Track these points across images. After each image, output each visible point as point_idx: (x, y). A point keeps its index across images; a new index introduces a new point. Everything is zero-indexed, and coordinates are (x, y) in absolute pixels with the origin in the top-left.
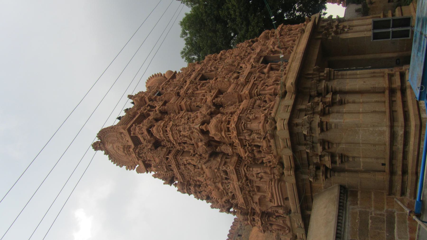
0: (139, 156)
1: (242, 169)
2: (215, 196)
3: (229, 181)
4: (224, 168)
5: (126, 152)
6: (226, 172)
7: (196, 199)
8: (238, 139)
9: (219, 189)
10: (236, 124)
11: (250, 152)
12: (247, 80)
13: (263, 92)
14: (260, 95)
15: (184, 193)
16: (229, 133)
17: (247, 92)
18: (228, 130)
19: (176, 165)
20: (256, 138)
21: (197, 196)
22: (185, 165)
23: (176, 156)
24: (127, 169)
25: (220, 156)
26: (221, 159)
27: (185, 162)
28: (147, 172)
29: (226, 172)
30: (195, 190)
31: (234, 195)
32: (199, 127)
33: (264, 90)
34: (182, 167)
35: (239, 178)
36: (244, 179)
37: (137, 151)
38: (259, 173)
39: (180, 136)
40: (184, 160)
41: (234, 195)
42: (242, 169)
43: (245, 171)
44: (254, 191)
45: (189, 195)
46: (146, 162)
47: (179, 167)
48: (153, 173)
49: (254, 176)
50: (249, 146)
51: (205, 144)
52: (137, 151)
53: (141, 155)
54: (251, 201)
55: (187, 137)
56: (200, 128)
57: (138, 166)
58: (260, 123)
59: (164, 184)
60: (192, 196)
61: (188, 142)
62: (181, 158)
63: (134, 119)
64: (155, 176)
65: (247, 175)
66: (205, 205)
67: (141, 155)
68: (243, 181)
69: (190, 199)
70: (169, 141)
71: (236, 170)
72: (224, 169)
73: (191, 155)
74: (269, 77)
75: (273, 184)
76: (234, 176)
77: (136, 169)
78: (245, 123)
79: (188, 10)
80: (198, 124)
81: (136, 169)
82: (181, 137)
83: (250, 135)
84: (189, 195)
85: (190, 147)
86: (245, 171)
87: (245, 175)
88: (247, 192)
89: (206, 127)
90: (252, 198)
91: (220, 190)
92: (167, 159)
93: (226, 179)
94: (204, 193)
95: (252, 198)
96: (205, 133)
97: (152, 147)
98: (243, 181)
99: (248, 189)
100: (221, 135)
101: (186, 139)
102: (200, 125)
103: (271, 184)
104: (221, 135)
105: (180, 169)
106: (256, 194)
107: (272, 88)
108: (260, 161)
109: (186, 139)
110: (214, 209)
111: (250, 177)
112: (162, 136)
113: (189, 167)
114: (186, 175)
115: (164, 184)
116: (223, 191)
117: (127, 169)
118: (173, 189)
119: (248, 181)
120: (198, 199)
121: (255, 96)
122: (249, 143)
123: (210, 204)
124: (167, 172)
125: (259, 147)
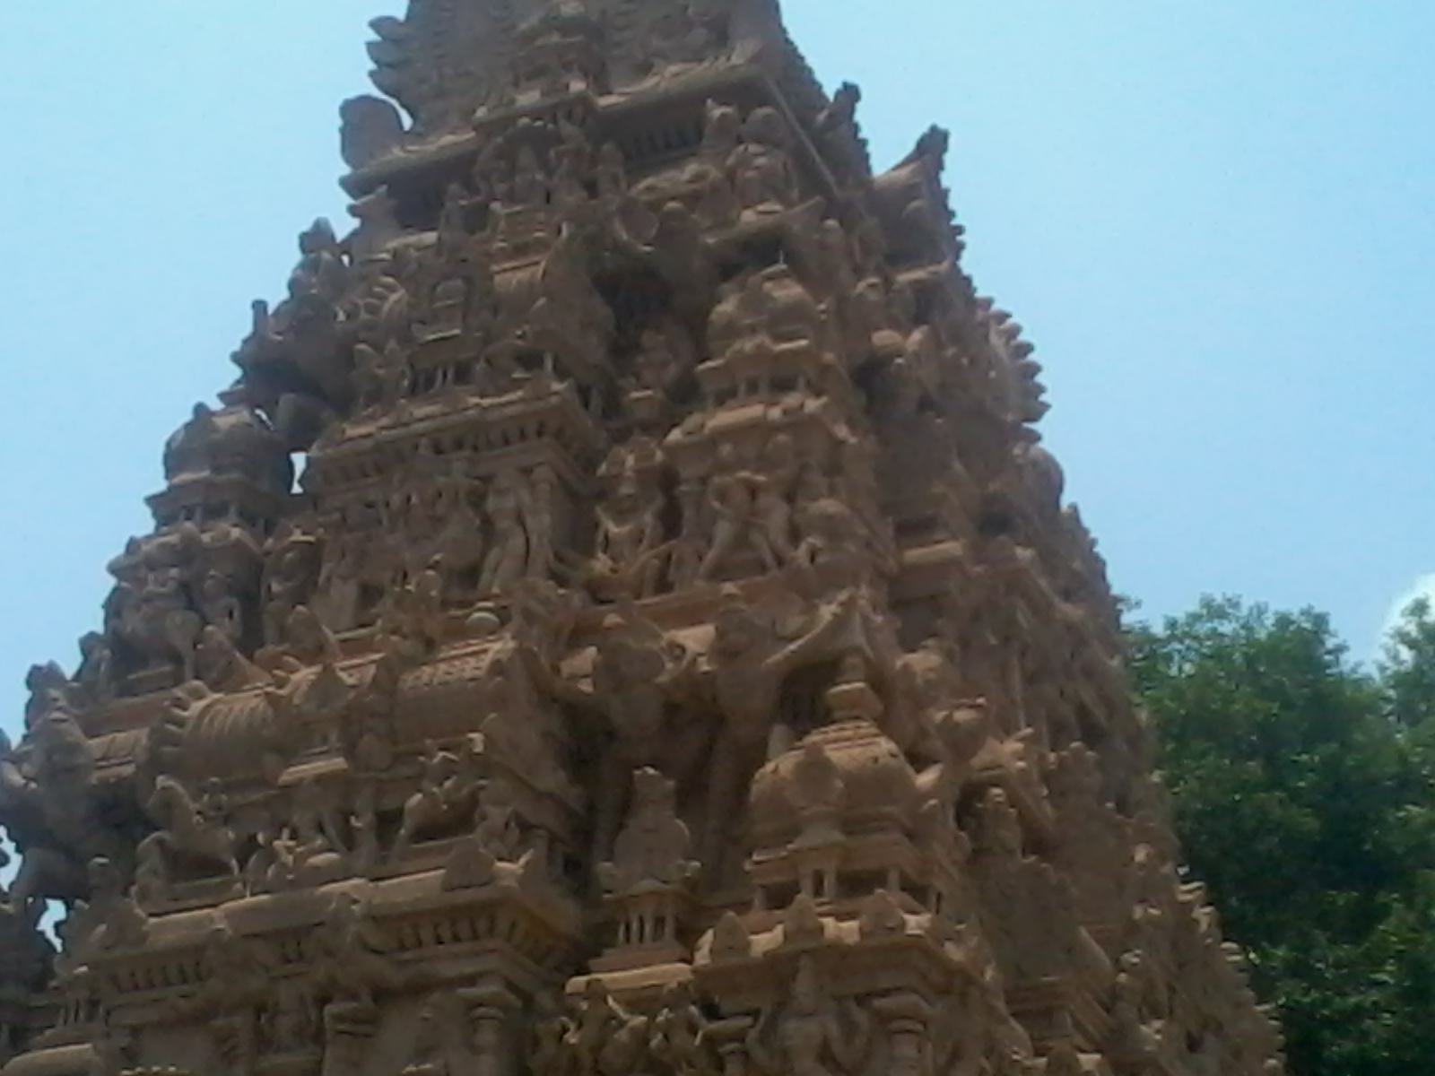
0: (514, 142)
1: (491, 963)
2: (197, 706)
4: (496, 815)
5: (555, 38)
6: (461, 819)
8: (796, 957)
15: (174, 458)
18: (856, 884)
21: (151, 564)
22: (477, 500)
23: (559, 434)
24: (376, 25)
26: (550, 795)
27: (509, 503)
28: (348, 184)
29: (461, 819)
32: (857, 650)
34: (458, 471)
35: (400, 928)
37: (567, 128)
39: (753, 491)
40: (526, 497)
42: (491, 963)
43: (471, 980)
46: (454, 188)
47: (459, 445)
48: (344, 226)
50: (710, 1040)
51: (694, 684)
52: (567, 128)
53: (526, 157)
54: (152, 1015)
55: (741, 541)
57: (407, 122)
59: (259, 306)
60: (143, 524)
61: (681, 547)
62: (542, 473)
63: (813, 151)
64: (315, 239)
65: (436, 997)
66: (61, 614)
67: (526, 157)
68: (377, 965)
69: (113, 501)
70: (685, 395)
71: (488, 909)
73: (559, 558)
76: (419, 883)
77: (376, 93)
79: (1369, 648)
81: (376, 93)
82: (740, 496)
86: (471, 980)
87: (418, 989)
89: (853, 701)
90: (200, 1018)
91: (270, 760)
92: (530, 360)
93: (387, 821)
95: (200, 1018)
96: (804, 697)
97: (618, 248)
98: (377, 965)
99: (285, 994)
101: (723, 531)
102: (867, 661)
105: (438, 450)
109: (723, 531)
113: (452, 531)
115: (259, 306)
117: (376, 25)
118: (207, 374)
119: (367, 1001)
122: (740, 1037)
123: (70, 664)
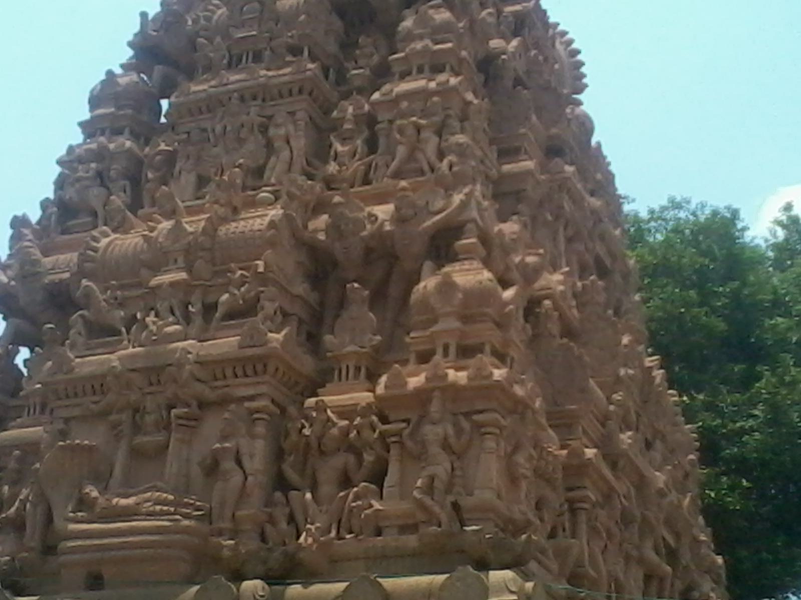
3: (198, 321)
4: (269, 307)
7: (62, 152)
8: (433, 390)
9: (156, 268)
10: (503, 389)
11: (346, 432)
12: (621, 463)
13: (583, 528)
14: (573, 511)
15: (95, 101)
16: (452, 350)
17: (365, 456)
19: (264, 87)
20: (430, 470)
21: (80, 160)
25: (313, 297)
27: (282, 131)
30: (113, 156)
31: (116, 333)
32: (474, 221)
33: (593, 531)
34: (254, 113)
35: (215, 368)
36: (209, 394)
38: (239, 462)
39: (418, 129)
41: (116, 333)
42: (263, 389)
43: (252, 398)
44: (137, 428)
45: (82, 125)
49: (224, 438)
51: (380, 235)
54: (76, 412)
55: (411, 157)
56: (468, 221)
58: (499, 496)
59: (144, 15)
61: (377, 159)
65: (233, 406)
68: (199, 387)
69: (63, 125)
70: (382, 74)
72: (267, 304)
73: (309, 163)
74: (628, 558)
75: (186, 522)
78: (501, 428)
80: (482, 217)
83: (446, 446)
84: (82, 125)
85: (356, 166)
86: (252, 398)
87: (223, 403)
88: (133, 397)
90: (103, 414)
91: (144, 272)
92: (296, 51)
93: (209, 309)
94: (95, 195)
99: (149, 403)
100: (448, 315)
101: (401, 151)
103: (186, 516)
104: (448, 315)
106: (118, 437)
107: (598, 571)
108: (292, 476)
109: (401, 151)
110: (9, 232)
111: (212, 425)
112: (419, 45)
113: (250, 146)
114: (208, 125)
115: (144, 15)
116: (139, 285)
118: (116, 55)
120: (60, 162)
121: (570, 489)
122: (399, 434)
123: (35, 215)
124: (226, 36)
125: (378, 477)
